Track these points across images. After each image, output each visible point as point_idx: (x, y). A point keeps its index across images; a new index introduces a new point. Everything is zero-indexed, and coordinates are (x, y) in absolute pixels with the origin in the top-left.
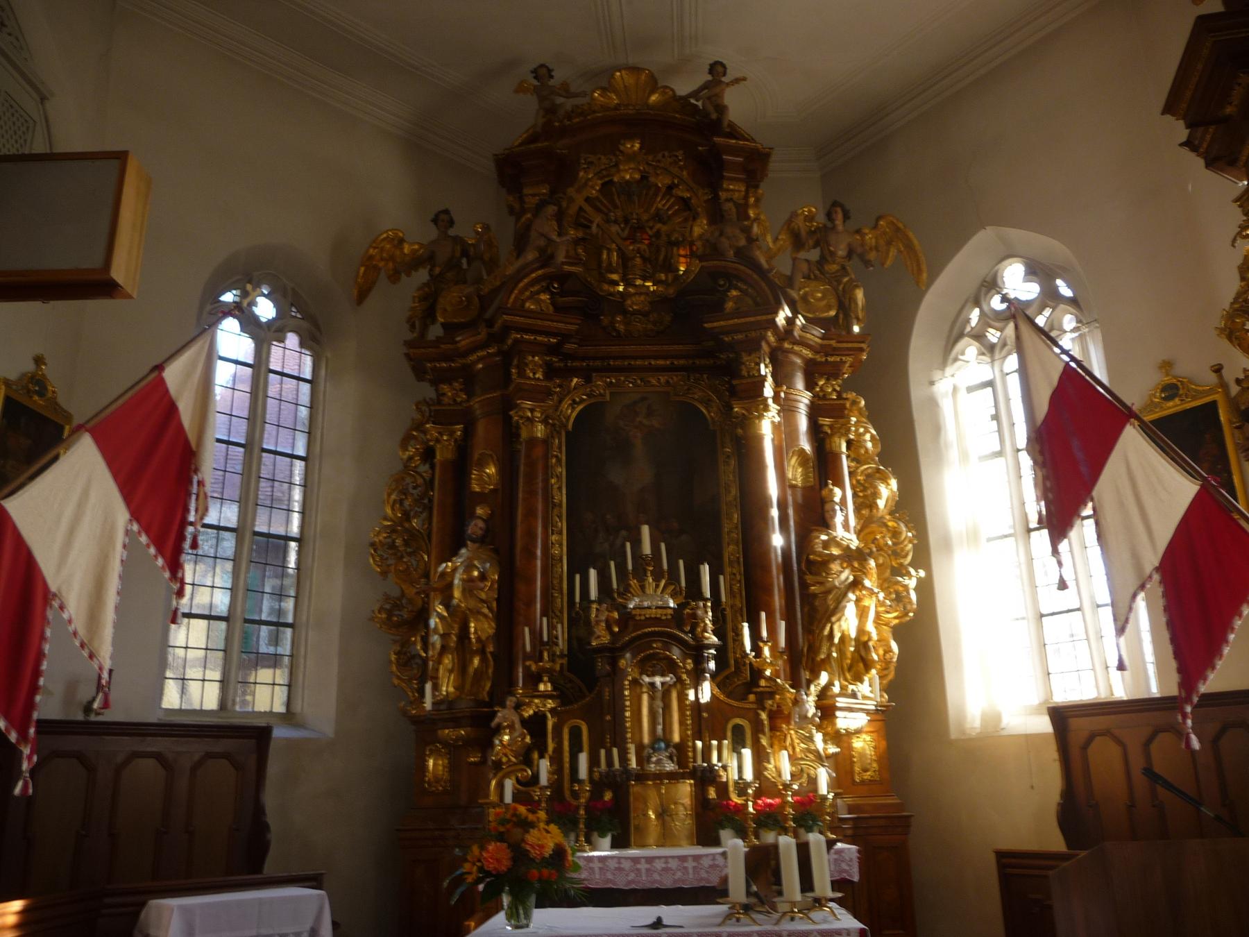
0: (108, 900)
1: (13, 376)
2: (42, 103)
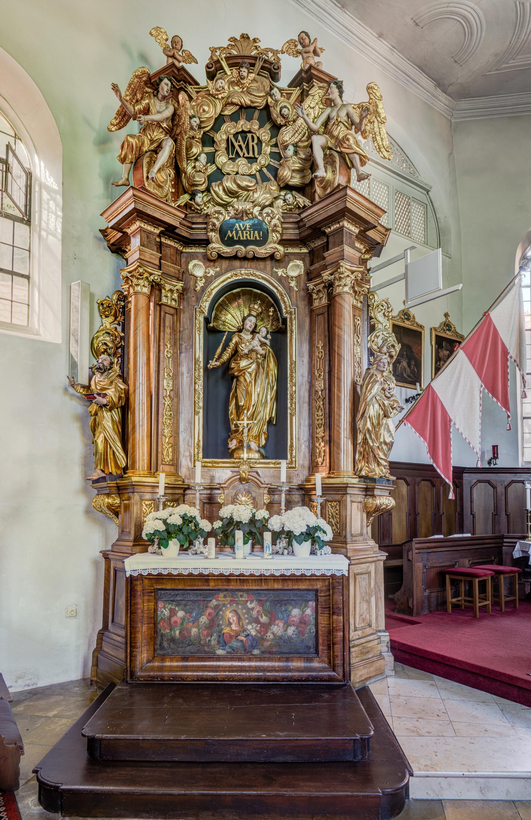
0: (505, 540)
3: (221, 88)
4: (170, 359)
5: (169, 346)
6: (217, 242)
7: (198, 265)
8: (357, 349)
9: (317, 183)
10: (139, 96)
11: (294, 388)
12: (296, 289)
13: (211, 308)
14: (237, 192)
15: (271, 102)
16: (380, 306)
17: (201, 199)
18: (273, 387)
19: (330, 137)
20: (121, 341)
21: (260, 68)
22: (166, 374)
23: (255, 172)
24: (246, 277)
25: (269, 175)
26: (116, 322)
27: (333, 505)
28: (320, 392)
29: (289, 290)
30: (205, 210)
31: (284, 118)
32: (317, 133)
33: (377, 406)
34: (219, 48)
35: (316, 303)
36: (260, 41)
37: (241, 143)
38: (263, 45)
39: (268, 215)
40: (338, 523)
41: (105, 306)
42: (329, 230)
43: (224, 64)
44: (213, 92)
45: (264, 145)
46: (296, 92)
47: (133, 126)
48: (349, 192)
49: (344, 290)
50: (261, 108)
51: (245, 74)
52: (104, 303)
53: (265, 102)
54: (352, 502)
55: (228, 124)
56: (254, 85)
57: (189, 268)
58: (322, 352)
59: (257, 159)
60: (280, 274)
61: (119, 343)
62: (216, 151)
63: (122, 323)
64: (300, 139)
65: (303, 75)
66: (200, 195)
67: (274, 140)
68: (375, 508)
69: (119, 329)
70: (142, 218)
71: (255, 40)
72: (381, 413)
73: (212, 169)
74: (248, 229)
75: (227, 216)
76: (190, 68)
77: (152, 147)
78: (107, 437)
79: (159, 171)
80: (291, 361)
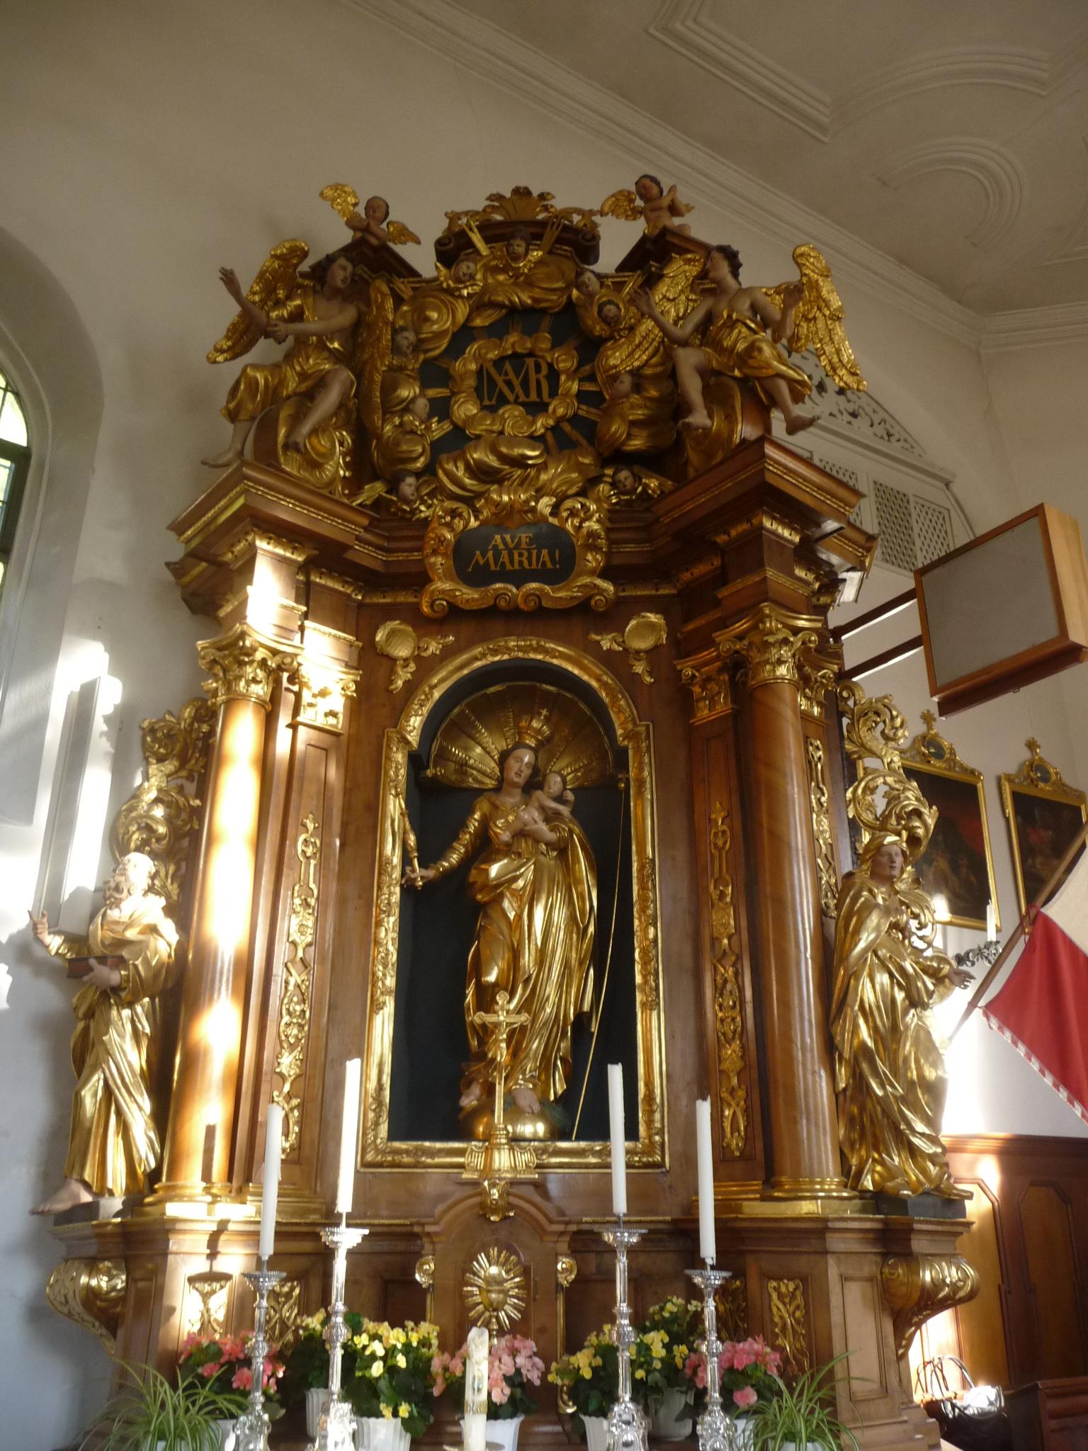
1: (1012, 769)
2: (948, 489)
3: (467, 277)
4: (313, 862)
5: (311, 826)
6: (447, 577)
7: (399, 630)
8: (819, 823)
9: (689, 444)
10: (281, 294)
11: (651, 931)
12: (649, 680)
13: (429, 730)
14: (498, 471)
15: (578, 298)
16: (870, 714)
17: (413, 488)
18: (586, 928)
19: (715, 351)
20: (191, 820)
21: (553, 240)
22: (297, 901)
23: (542, 431)
24: (520, 655)
25: (576, 435)
26: (184, 773)
27: (783, 1289)
28: (726, 941)
29: (629, 682)
30: (421, 511)
31: (608, 324)
32: (684, 343)
33: (883, 979)
34: (466, 213)
35: (704, 713)
36: (554, 197)
37: (512, 376)
38: (559, 204)
39: (573, 513)
40: (803, 1354)
41: (159, 734)
42: (724, 537)
43: (476, 238)
44: (448, 285)
45: (563, 378)
46: (632, 282)
47: (264, 350)
48: (770, 450)
49: (778, 673)
50: (557, 310)
51: (521, 250)
52: (157, 727)
53: (564, 299)
54: (844, 1279)
55: (481, 342)
56: (541, 271)
57: (377, 638)
58: (724, 832)
59: (547, 405)
60: (606, 645)
61: (185, 825)
62: (453, 394)
63: (200, 774)
64: (647, 361)
65: (649, 246)
66: (410, 480)
67: (587, 368)
68: (921, 1298)
69: (191, 788)
70: (259, 528)
71: (542, 196)
72: (900, 996)
73: (438, 429)
74: (523, 546)
75: (472, 519)
76: (405, 251)
77: (303, 387)
78: (111, 1082)
79: (314, 432)
80: (640, 860)
